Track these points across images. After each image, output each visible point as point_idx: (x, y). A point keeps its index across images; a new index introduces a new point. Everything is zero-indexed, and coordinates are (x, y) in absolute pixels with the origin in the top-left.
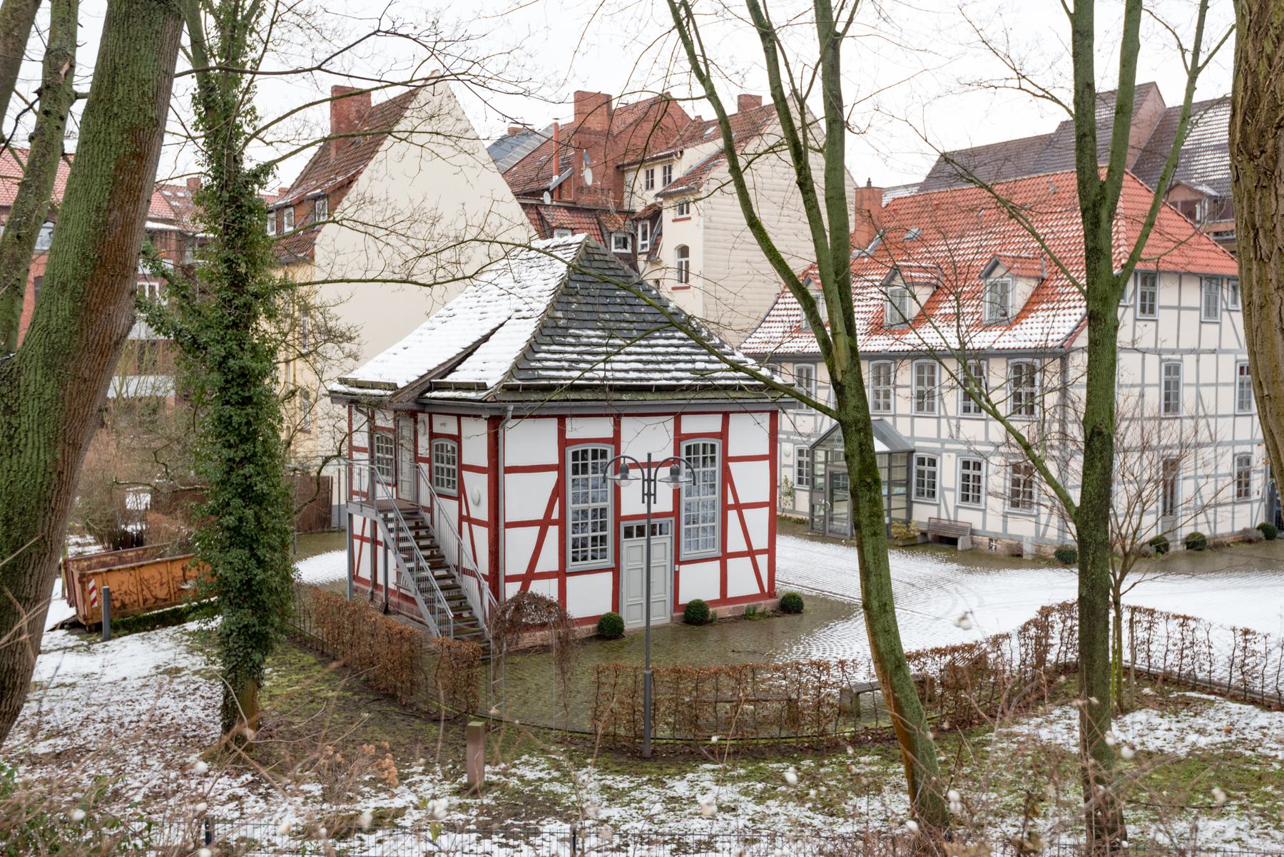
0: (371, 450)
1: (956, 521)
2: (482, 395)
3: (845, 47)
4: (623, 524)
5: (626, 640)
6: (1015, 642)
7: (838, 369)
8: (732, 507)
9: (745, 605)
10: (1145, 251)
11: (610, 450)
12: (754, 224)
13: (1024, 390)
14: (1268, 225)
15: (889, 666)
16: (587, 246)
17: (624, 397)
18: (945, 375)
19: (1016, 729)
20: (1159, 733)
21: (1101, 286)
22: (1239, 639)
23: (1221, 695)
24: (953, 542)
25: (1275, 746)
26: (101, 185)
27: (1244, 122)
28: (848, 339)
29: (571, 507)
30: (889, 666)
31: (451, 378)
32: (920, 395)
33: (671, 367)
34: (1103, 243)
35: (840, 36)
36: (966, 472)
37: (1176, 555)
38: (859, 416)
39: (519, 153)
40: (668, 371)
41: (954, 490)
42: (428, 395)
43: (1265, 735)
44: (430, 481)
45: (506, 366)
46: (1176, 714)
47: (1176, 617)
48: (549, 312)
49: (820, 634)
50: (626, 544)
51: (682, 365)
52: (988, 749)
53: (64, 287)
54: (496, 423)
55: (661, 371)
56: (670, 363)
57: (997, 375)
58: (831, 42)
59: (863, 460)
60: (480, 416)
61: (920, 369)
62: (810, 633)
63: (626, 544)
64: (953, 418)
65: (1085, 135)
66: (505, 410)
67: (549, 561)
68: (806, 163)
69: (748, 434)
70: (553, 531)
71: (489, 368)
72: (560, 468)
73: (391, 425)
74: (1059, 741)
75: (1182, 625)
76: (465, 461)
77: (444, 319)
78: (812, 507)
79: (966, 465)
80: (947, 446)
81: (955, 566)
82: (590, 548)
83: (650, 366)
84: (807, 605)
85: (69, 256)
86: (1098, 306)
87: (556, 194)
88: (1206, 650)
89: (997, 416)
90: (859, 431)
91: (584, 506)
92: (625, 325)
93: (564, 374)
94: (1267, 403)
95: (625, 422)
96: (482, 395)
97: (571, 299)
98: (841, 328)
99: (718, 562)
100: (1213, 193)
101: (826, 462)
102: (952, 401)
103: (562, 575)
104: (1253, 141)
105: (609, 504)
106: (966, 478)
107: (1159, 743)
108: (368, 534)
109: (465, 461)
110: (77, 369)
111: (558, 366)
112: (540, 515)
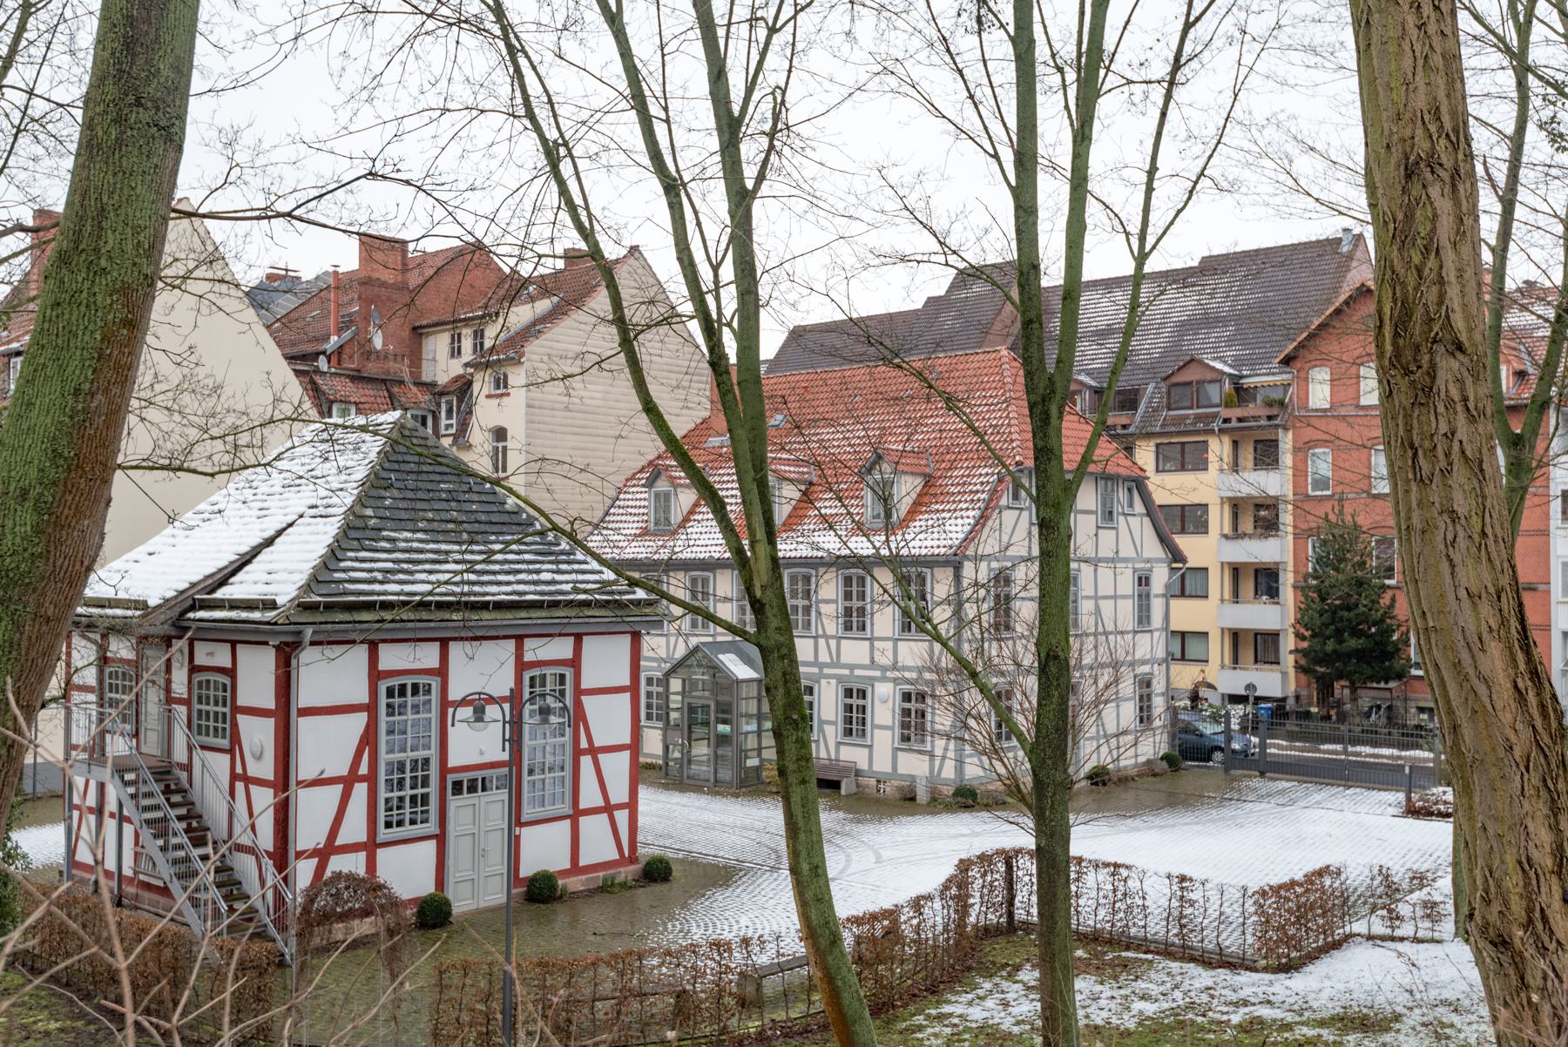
0: (100, 690)
1: (837, 760)
2: (270, 615)
3: (760, 210)
4: (451, 778)
5: (454, 927)
6: (937, 905)
7: (757, 584)
8: (585, 752)
9: (601, 874)
10: (1097, 452)
11: (435, 684)
12: (650, 408)
13: (855, 604)
14: (1427, 444)
15: (823, 943)
16: (403, 427)
17: (454, 617)
18: (877, 590)
19: (947, 1009)
20: (1103, 1003)
21: (1054, 489)
22: (1175, 888)
23: (1157, 953)
24: (835, 785)
25: (1225, 1009)
26: (82, 360)
27: (1396, 335)
28: (769, 548)
29: (384, 757)
30: (823, 943)
31: (222, 593)
32: (848, 612)
33: (511, 578)
34: (1053, 442)
35: (752, 195)
36: (849, 701)
37: (1079, 791)
38: (782, 639)
39: (283, 307)
40: (508, 583)
41: (834, 723)
42: (191, 615)
43: (1212, 997)
44: (189, 726)
45: (301, 579)
46: (1116, 978)
47: (1107, 865)
48: (357, 509)
49: (698, 906)
50: (454, 803)
51: (522, 576)
52: (919, 1035)
53: (24, 494)
54: (286, 655)
55: (499, 583)
56: (512, 577)
58: (741, 200)
59: (788, 693)
60: (266, 643)
61: (848, 581)
62: (685, 906)
63: (454, 803)
64: (832, 637)
65: (1031, 321)
66: (300, 633)
67: (354, 829)
68: (720, 339)
69: (605, 660)
70: (360, 790)
71: (281, 578)
72: (371, 708)
73: (131, 656)
74: (996, 1021)
75: (1113, 875)
76: (241, 702)
77: (206, 516)
78: (666, 748)
79: (849, 693)
80: (826, 671)
81: (841, 814)
82: (408, 810)
83: (486, 578)
84: (677, 872)
85: (32, 453)
86: (1049, 513)
87: (334, 360)
88: (1140, 902)
89: (937, 637)
90: (782, 658)
91: (401, 756)
92: (451, 526)
93: (377, 587)
94: (1433, 636)
95: (455, 649)
96: (270, 615)
97: (383, 493)
98: (761, 534)
99: (567, 823)
100: (1093, 383)
101: (683, 693)
102: (885, 620)
103: (371, 847)
104: (1408, 354)
105: (433, 753)
107: (1105, 1014)
108: (91, 801)
109: (241, 702)
110: (39, 605)
111: (367, 576)
112: (343, 770)
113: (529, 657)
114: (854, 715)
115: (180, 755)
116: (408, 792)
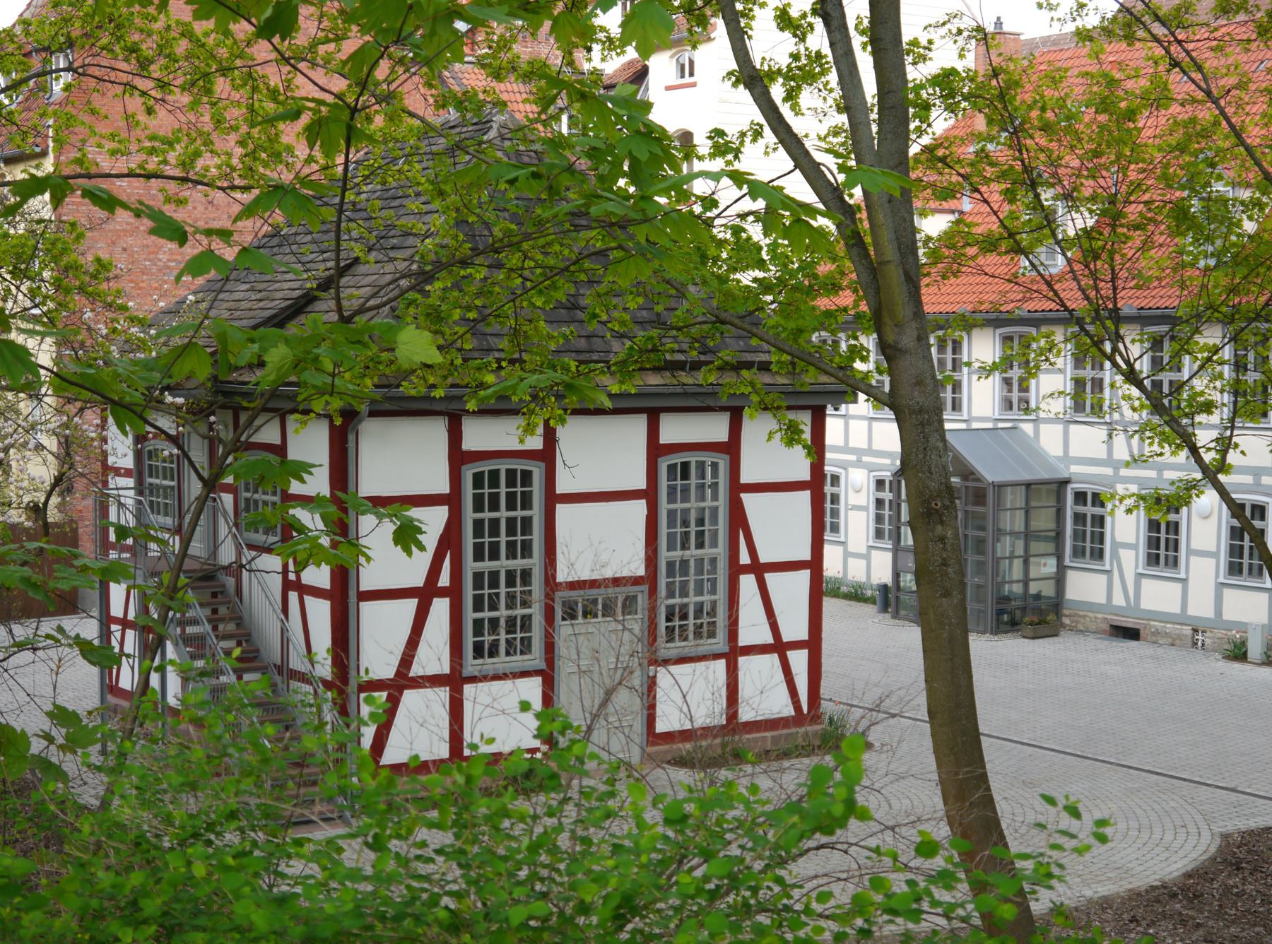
8: (746, 569)
11: (537, 471)
29: (470, 566)
41: (1134, 547)
63: (564, 630)
67: (434, 655)
70: (441, 607)
103: (454, 681)
112: (418, 581)
113: (664, 439)
114: (1163, 535)
115: (227, 554)
116: (503, 613)
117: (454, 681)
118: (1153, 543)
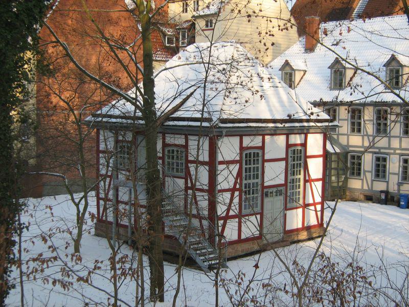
42: (167, 124)
57: (369, 115)
66: (222, 132)
70: (237, 193)
79: (378, 159)
106: (378, 166)
113: (245, 145)
117: (239, 216)
118: (378, 171)
